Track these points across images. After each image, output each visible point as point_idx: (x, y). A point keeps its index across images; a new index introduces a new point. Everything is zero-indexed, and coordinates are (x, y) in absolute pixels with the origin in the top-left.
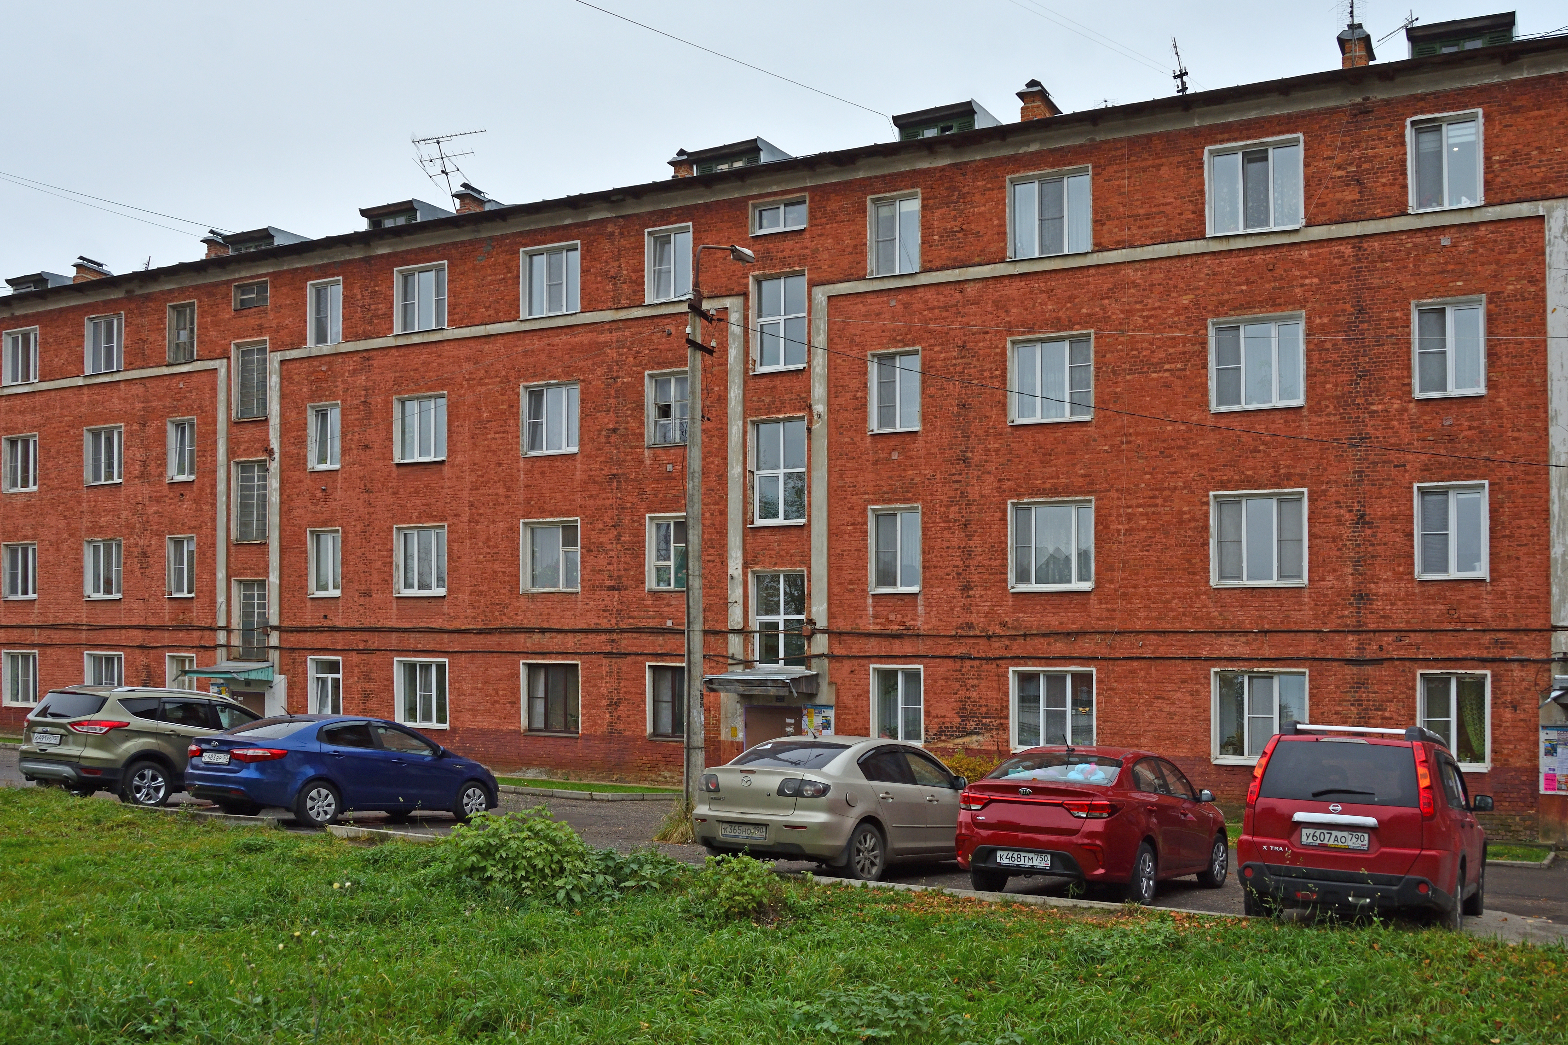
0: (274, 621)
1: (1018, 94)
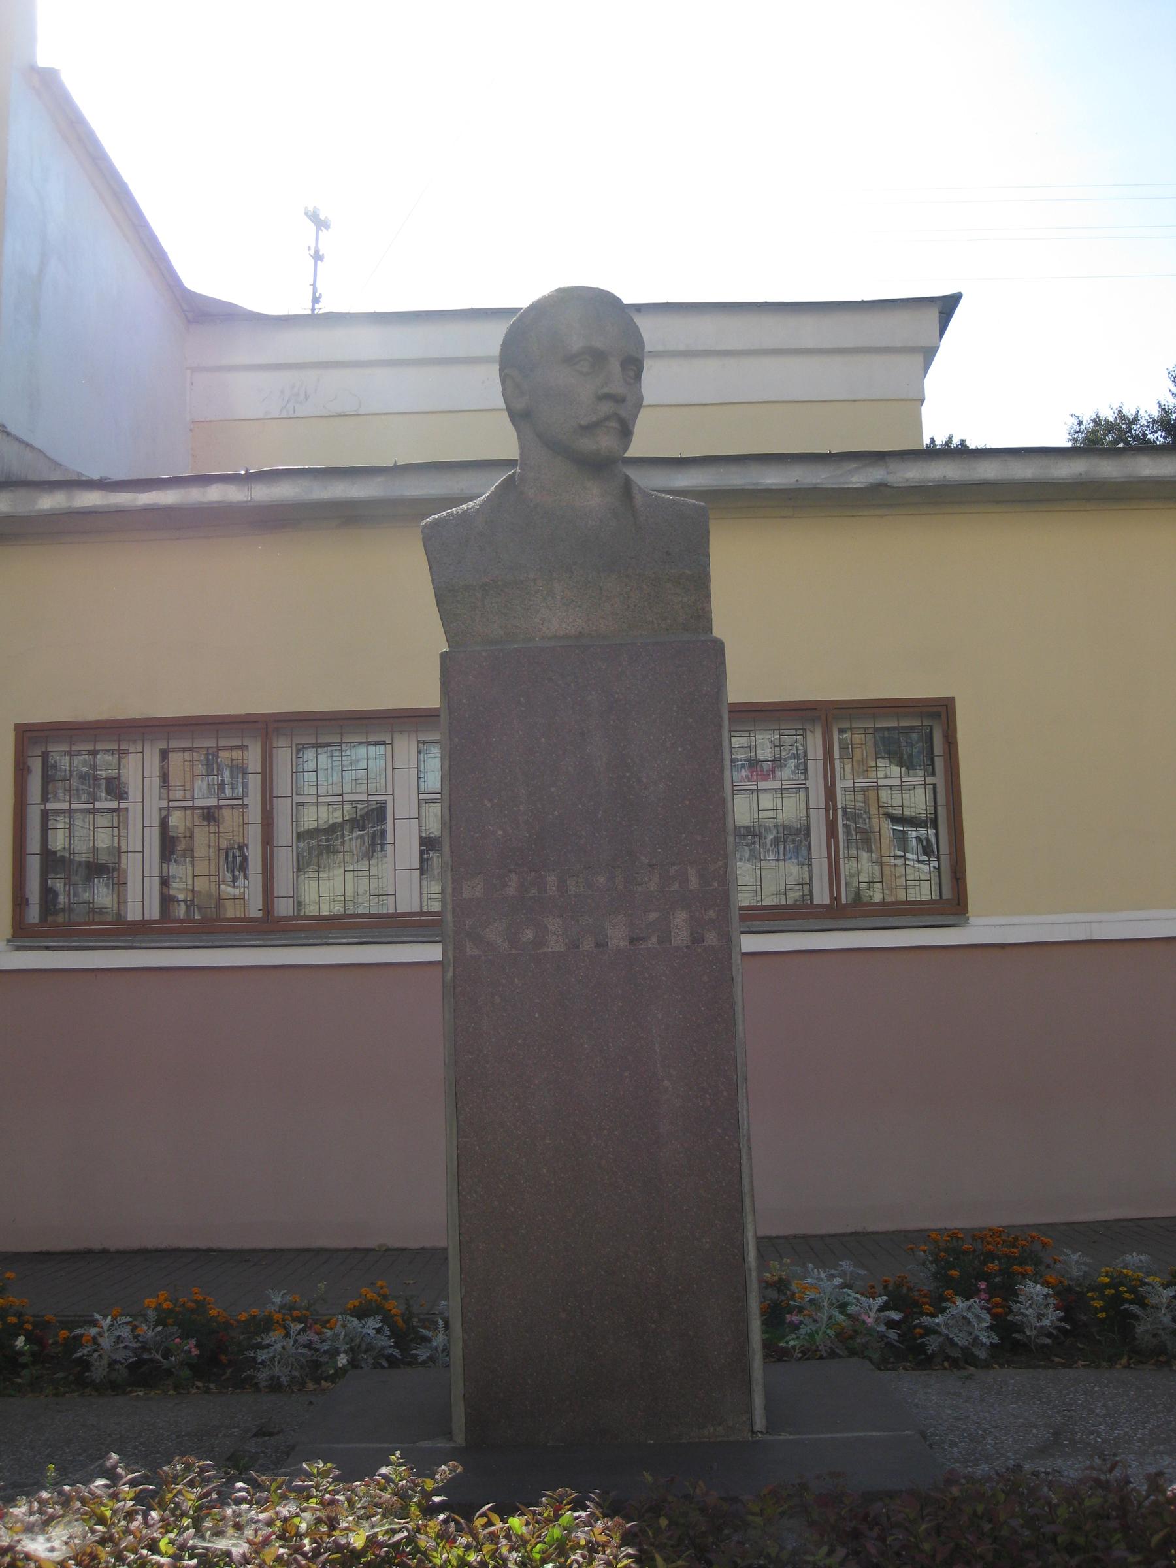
0: (294, 771)
1: (947, 306)
